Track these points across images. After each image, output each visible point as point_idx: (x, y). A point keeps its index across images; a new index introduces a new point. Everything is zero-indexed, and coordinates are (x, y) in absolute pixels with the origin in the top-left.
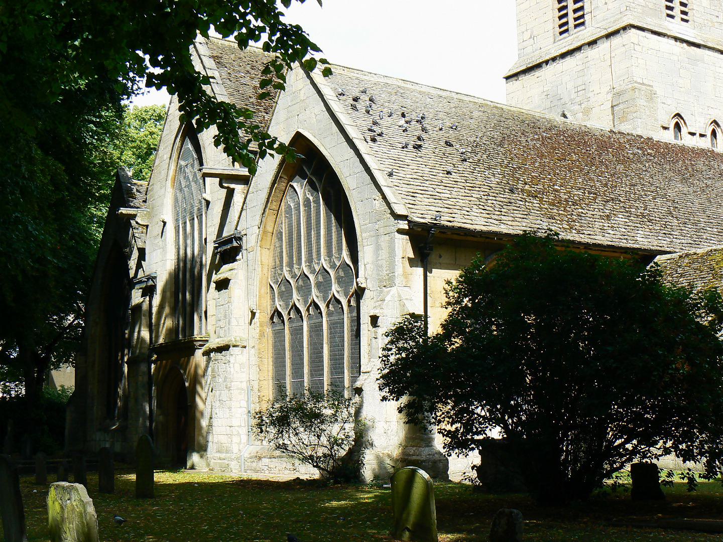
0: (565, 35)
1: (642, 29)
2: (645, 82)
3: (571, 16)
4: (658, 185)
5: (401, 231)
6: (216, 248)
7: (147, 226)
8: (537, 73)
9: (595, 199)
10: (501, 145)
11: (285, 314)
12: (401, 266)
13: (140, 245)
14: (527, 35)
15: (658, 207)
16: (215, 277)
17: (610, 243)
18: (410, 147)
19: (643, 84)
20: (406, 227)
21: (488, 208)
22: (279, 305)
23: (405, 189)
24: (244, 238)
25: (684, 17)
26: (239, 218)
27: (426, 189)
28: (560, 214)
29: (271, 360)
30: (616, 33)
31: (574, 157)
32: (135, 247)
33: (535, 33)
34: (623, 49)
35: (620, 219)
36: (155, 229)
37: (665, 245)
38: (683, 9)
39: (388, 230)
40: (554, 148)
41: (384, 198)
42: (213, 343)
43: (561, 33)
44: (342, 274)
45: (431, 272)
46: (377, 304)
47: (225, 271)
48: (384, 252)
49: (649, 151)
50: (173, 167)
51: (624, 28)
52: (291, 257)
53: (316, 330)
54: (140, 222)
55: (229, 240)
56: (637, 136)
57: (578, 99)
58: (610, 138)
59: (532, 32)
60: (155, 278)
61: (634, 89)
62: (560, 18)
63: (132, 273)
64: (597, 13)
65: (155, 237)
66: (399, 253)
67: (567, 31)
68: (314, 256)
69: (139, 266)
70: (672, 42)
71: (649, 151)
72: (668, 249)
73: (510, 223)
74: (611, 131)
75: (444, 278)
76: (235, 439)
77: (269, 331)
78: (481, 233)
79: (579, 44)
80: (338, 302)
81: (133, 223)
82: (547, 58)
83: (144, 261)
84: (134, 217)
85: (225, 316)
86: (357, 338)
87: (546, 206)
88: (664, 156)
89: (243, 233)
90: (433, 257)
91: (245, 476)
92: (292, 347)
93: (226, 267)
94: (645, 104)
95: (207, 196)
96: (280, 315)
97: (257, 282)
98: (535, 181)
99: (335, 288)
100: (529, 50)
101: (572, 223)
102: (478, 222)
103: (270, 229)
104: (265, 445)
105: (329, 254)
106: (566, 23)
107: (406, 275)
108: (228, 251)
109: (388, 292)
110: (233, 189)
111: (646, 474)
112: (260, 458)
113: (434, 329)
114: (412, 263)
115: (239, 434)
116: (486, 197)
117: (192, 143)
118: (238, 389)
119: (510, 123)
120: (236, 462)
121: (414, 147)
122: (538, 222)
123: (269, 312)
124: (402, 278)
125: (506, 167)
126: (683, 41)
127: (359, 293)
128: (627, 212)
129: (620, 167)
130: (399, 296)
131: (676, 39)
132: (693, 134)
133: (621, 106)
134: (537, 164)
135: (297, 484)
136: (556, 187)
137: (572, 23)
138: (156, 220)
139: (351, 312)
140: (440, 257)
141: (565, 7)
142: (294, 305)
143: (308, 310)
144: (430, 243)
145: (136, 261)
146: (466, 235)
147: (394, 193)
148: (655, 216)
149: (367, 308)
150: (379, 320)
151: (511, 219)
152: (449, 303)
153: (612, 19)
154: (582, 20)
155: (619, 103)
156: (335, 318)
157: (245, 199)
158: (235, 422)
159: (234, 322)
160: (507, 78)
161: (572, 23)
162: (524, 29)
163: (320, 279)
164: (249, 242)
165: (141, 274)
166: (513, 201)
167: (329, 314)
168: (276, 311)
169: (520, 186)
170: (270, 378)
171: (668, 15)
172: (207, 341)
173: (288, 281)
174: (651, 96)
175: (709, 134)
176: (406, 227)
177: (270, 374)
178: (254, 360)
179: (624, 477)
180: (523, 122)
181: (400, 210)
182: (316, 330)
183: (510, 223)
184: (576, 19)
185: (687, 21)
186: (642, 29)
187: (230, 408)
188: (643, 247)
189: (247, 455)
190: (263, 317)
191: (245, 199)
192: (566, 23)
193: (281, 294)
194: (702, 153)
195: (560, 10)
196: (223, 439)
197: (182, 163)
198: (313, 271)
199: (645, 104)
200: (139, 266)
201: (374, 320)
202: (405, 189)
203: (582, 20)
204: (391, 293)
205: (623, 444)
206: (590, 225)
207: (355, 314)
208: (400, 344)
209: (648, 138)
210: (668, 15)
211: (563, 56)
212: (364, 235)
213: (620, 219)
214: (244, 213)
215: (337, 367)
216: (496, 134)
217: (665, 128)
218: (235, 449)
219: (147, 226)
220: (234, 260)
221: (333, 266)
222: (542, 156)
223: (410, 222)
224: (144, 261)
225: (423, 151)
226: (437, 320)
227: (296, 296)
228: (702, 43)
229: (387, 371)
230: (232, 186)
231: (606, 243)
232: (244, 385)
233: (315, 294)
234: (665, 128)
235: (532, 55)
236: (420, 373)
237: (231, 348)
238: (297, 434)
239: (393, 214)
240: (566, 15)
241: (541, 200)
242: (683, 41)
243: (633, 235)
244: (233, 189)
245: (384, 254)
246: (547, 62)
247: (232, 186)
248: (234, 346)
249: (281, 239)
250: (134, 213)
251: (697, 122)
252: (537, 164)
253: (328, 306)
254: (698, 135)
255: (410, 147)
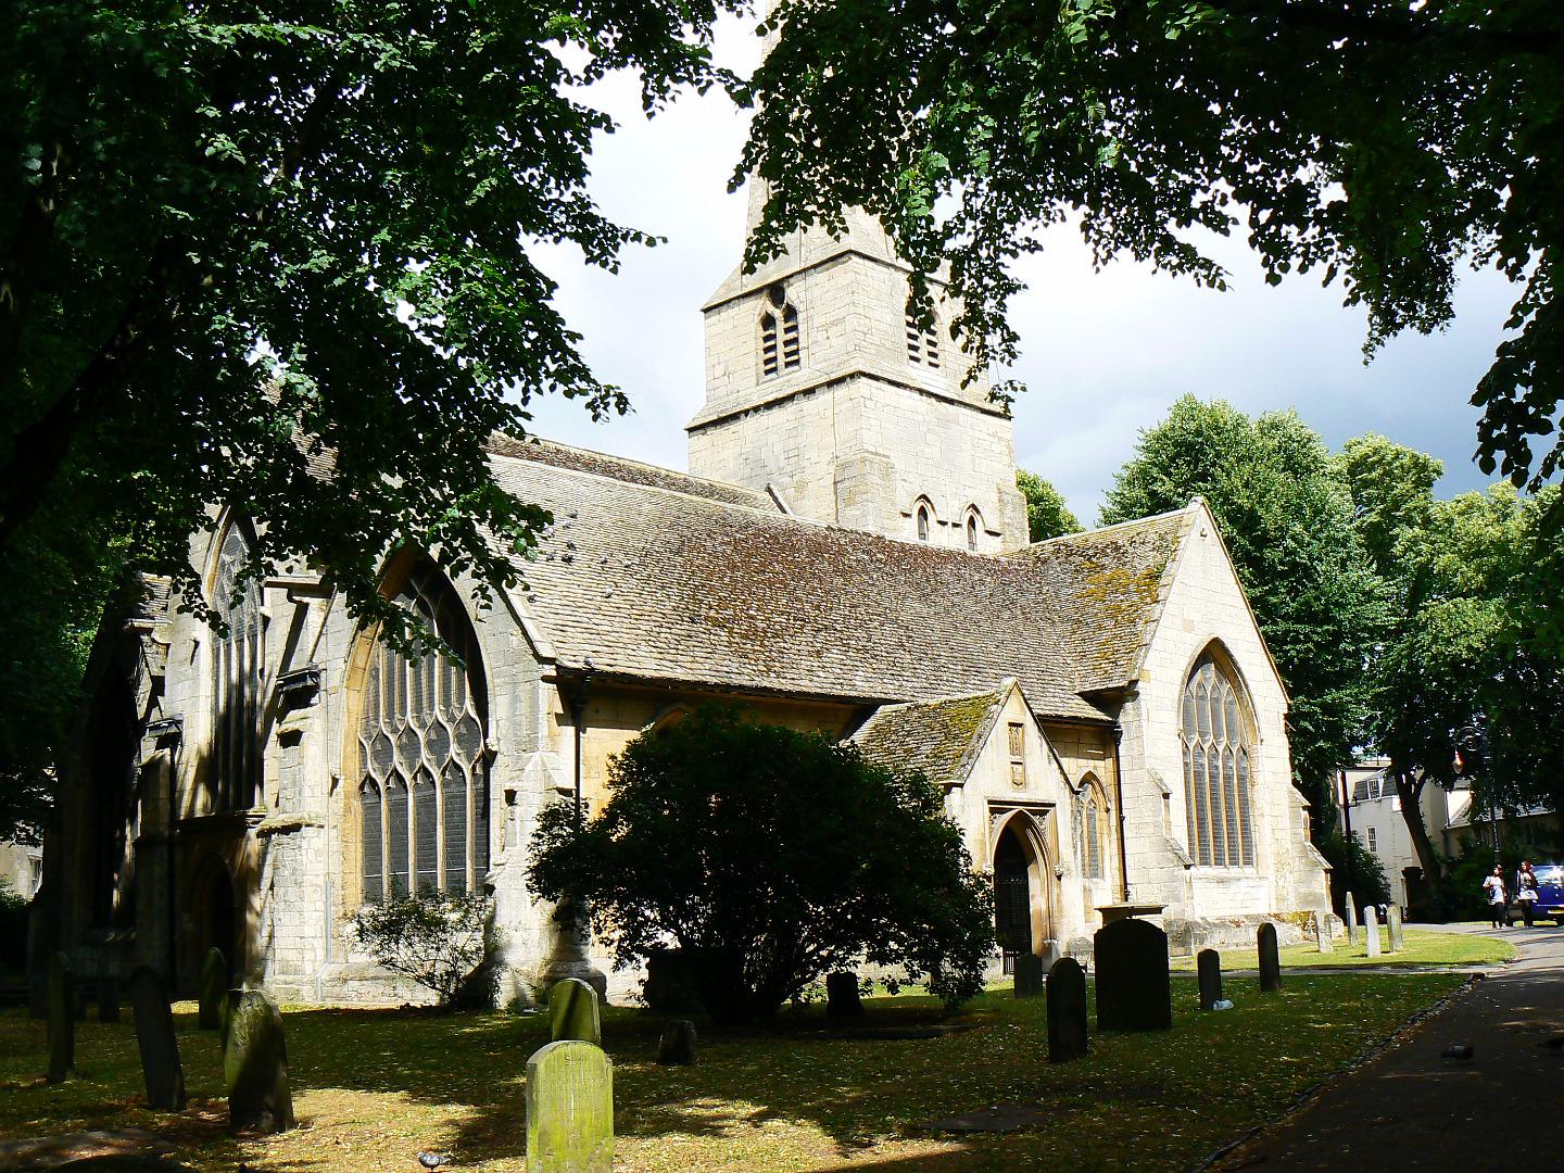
0: (773, 375)
1: (876, 378)
2: (880, 451)
3: (781, 349)
4: (887, 605)
5: (546, 679)
6: (278, 687)
7: (168, 646)
8: (733, 426)
9: (803, 627)
10: (679, 553)
11: (380, 781)
12: (546, 724)
13: (156, 671)
14: (719, 371)
15: (887, 636)
16: (276, 728)
17: (818, 691)
18: (558, 559)
19: (877, 454)
20: (554, 673)
21: (659, 644)
22: (372, 768)
23: (553, 619)
24: (323, 674)
25: (933, 360)
26: (316, 646)
27: (578, 619)
28: (755, 651)
29: (359, 845)
30: (840, 381)
31: (778, 568)
32: (146, 673)
33: (731, 369)
34: (850, 404)
35: (835, 655)
36: (181, 651)
37: (888, 689)
38: (932, 349)
39: (529, 676)
40: (751, 555)
41: (525, 633)
42: (274, 819)
43: (767, 372)
44: (463, 730)
45: (584, 732)
46: (514, 774)
47: (294, 720)
48: (522, 706)
49: (879, 556)
50: (211, 563)
51: (852, 376)
52: (390, 705)
53: (426, 805)
54: (157, 639)
55: (301, 677)
56: (865, 534)
57: (788, 469)
58: (826, 537)
59: (726, 367)
60: (181, 722)
61: (864, 461)
62: (767, 350)
63: (141, 712)
64: (817, 349)
65: (181, 663)
66: (544, 708)
67: (774, 370)
68: (425, 703)
69: (153, 703)
70: (916, 395)
71: (879, 556)
72: (895, 697)
73: (688, 665)
74: (829, 528)
75: (609, 742)
76: (309, 955)
77: (357, 805)
78: (653, 680)
79: (791, 391)
80: (460, 769)
81: (145, 638)
82: (747, 407)
83: (163, 695)
84: (149, 631)
85: (294, 783)
86: (483, 818)
87: (737, 640)
88: (898, 562)
89: (320, 667)
90: (588, 712)
91: (329, 1004)
92: (392, 828)
93: (293, 714)
94: (879, 482)
95: (266, 610)
96: (374, 783)
97: (341, 737)
98: (723, 604)
99: (454, 750)
100: (722, 391)
101: (771, 663)
102: (647, 665)
103: (361, 664)
104: (363, 957)
105: (447, 703)
106: (774, 359)
107: (552, 736)
108: (299, 691)
109: (529, 759)
110: (307, 604)
111: (844, 986)
112: (345, 981)
113: (593, 815)
114: (561, 720)
115: (313, 949)
116: (657, 629)
117: (242, 531)
118: (312, 885)
119: (692, 519)
120: (309, 987)
121: (563, 560)
122: (726, 663)
123: (359, 780)
124: (548, 740)
125: (685, 586)
126: (930, 395)
127: (489, 758)
128: (844, 645)
129: (838, 581)
130: (543, 763)
131: (921, 392)
132: (943, 523)
133: (847, 483)
134: (727, 580)
135: (407, 1011)
136: (751, 612)
137: (782, 360)
138: (182, 637)
139: (475, 782)
140: (597, 711)
141: (773, 337)
142: (395, 770)
143: (415, 778)
144: (586, 695)
145: (148, 695)
146: (630, 683)
147: (537, 627)
148: (881, 650)
149: (500, 780)
150: (517, 796)
151: (690, 659)
152: (612, 783)
153: (836, 361)
154: (795, 357)
155: (844, 484)
156: (454, 788)
157: (326, 619)
158: (308, 931)
159: (307, 791)
160: (690, 430)
161: (782, 360)
162: (716, 362)
163: (433, 736)
164: (332, 678)
165: (155, 716)
166: (693, 634)
167: (445, 784)
168: (369, 777)
169: (703, 612)
170: (359, 870)
171: (912, 358)
172: (263, 816)
173: (387, 737)
174: (888, 471)
175: (965, 523)
176: (554, 673)
177: (359, 865)
178: (335, 845)
179: (816, 990)
180: (709, 517)
181: (546, 652)
182: (426, 805)
183: (688, 665)
184: (787, 355)
185: (937, 366)
186: (876, 378)
187: (301, 912)
188: (863, 695)
189: (325, 977)
190: (349, 784)
191: (326, 619)
192: (774, 359)
193: (376, 754)
194: (949, 557)
195: (766, 339)
196: (291, 956)
197: (227, 558)
198: (423, 725)
199: (879, 482)
200: (153, 703)
201: (511, 796)
202: (553, 619)
203: (795, 357)
204: (533, 760)
205: (816, 951)
206: (793, 665)
207: (481, 785)
208: (556, 830)
209: (878, 537)
210: (912, 358)
211: (769, 405)
212: (497, 681)
213: (835, 655)
214: (323, 639)
215: (455, 856)
216: (673, 537)
217: (906, 515)
218: (308, 968)
219: (168, 646)
220: (307, 704)
221: (452, 719)
222: (734, 568)
223: (559, 668)
224: (163, 695)
225: (576, 565)
226: (598, 797)
227: (397, 758)
228: (956, 398)
229: (536, 863)
230: (306, 600)
231: (813, 690)
232: (321, 880)
233: (425, 756)
234: (906, 515)
235: (726, 399)
236: (575, 869)
237: (303, 828)
238: (410, 944)
239: (536, 655)
240: (773, 348)
241: (731, 632)
242: (930, 395)
243: (849, 677)
244: (307, 604)
245: (523, 708)
246: (746, 412)
247: (306, 600)
248: (308, 826)
249: (376, 678)
250: (150, 625)
251: (949, 507)
252: (727, 580)
253: (443, 774)
254: (950, 524)
255: (558, 559)
